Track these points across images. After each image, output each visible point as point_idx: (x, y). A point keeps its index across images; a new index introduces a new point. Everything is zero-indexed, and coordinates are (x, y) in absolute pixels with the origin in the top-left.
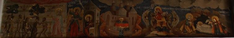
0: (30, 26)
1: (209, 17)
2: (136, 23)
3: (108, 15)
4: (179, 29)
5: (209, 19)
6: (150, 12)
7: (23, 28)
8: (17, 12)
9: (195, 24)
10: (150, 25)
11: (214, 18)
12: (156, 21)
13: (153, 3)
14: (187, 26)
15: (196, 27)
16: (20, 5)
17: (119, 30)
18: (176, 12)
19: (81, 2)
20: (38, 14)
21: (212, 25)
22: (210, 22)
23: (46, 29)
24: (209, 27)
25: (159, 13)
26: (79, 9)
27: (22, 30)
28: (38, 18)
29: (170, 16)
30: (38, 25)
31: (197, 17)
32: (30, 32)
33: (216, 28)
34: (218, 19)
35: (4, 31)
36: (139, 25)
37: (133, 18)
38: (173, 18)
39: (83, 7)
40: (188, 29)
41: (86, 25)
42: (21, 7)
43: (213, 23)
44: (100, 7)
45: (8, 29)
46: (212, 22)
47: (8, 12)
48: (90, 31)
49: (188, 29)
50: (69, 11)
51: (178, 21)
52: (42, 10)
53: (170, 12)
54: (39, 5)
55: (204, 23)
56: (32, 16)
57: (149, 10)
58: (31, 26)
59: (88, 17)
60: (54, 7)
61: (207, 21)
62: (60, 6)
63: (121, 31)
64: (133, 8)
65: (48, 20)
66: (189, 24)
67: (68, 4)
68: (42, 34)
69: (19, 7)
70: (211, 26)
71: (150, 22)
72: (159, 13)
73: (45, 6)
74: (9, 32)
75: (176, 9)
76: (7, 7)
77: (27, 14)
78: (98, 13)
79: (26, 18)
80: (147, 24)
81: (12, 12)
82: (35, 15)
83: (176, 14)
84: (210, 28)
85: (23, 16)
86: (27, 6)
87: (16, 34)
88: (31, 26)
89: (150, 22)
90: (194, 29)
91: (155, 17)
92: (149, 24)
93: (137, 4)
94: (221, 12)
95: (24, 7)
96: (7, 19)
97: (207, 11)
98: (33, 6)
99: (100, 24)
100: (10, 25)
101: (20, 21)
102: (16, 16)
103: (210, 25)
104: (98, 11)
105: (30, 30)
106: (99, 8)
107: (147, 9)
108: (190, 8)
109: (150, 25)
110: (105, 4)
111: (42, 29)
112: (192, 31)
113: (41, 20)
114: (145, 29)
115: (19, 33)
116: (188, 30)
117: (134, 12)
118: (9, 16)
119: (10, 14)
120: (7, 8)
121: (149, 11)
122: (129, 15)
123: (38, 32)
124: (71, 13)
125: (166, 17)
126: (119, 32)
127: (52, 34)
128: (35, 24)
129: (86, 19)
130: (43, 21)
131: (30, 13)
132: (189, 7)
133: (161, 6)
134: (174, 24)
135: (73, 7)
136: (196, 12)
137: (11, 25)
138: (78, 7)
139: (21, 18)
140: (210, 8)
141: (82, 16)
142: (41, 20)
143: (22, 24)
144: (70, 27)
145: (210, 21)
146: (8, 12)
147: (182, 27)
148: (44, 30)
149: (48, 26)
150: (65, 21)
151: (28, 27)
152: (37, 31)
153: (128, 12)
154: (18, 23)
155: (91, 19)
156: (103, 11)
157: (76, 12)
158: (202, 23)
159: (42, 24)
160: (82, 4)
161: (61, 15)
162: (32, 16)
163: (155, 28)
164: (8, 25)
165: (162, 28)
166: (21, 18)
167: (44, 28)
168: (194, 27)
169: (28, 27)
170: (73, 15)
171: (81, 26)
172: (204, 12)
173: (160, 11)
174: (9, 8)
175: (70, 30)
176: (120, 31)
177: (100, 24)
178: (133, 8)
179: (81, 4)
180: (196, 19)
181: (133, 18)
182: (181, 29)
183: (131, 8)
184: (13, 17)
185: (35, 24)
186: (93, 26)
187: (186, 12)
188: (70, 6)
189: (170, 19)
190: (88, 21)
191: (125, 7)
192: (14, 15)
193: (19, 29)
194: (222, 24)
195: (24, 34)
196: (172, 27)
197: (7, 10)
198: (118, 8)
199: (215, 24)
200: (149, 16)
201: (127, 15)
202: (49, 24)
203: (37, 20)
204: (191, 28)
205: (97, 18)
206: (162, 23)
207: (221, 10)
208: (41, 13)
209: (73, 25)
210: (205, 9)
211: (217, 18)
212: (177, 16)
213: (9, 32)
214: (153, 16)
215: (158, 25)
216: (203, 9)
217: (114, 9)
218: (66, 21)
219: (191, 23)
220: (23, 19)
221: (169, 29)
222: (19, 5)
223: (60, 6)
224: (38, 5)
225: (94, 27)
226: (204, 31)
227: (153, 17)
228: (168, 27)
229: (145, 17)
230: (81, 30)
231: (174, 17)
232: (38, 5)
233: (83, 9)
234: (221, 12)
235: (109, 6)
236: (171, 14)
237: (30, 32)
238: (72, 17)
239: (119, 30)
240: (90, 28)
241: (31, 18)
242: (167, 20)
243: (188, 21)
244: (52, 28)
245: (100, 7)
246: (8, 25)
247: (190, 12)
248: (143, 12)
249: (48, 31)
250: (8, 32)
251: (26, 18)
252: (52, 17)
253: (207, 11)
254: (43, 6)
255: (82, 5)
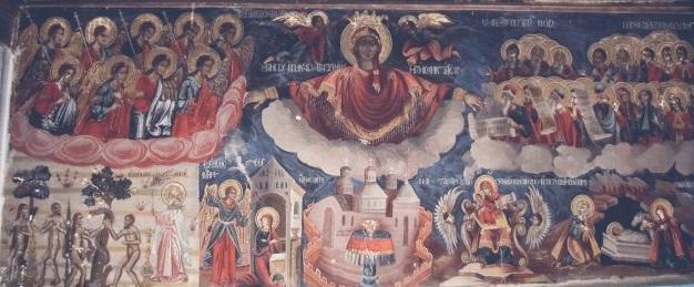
0: (86, 242)
1: (643, 205)
2: (416, 236)
3: (329, 210)
4: (550, 253)
5: (643, 211)
6: (459, 197)
7: (68, 249)
8: (46, 193)
9: (599, 229)
10: (460, 241)
11: (658, 209)
12: (477, 228)
13: (472, 161)
14: (575, 243)
15: (600, 244)
16: (54, 168)
17: (362, 262)
18: (541, 192)
19: (243, 162)
20: (109, 201)
21: (652, 233)
22: (645, 222)
23: (136, 254)
24: (642, 238)
25: (487, 198)
26: (172, 59)
27: (65, 257)
28: (109, 216)
29: (521, 210)
30: (110, 240)
31: (605, 207)
32: (90, 265)
33: (663, 243)
34: (670, 211)
35: (9, 259)
36: (425, 244)
37: (406, 220)
38: (532, 215)
39: (248, 179)
40: (576, 250)
41: (260, 245)
42: (58, 176)
43: (657, 225)
44: (303, 180)
45: (20, 252)
46: (650, 220)
47: (18, 194)
48: (272, 266)
49: (576, 250)
50: (206, 194)
51: (547, 224)
52: (121, 189)
53: (522, 193)
54: (112, 170)
55: (627, 226)
56: (92, 208)
57: (459, 190)
58: (90, 243)
59: (265, 217)
60: (157, 180)
61: (637, 219)
62: (176, 174)
63: (368, 266)
64: (407, 183)
65: (142, 222)
66: (582, 233)
67: (202, 170)
68: (124, 273)
69: (50, 175)
70: (649, 237)
71: (459, 231)
72: (489, 200)
73: (129, 175)
74: (24, 262)
75: (542, 182)
76: (18, 174)
77: (78, 203)
78: (296, 203)
79: (72, 216)
80: (450, 239)
81: (32, 195)
82: (101, 203)
83: (541, 198)
84: (646, 243)
85: (64, 208)
86: (77, 173)
87: (44, 269)
88: (90, 243)
89: (459, 231)
90: (596, 251)
91: (477, 213)
92: (455, 241)
93: (420, 170)
94: (680, 185)
95: (67, 176)
96: (18, 217)
97: (639, 183)
98: (94, 175)
99: (305, 241)
100: (26, 239)
101: (58, 226)
102: (44, 205)
103: (646, 232)
104: (295, 196)
105: (89, 254)
106: (301, 185)
107: (452, 187)
108: (586, 177)
109: (460, 241)
110: (318, 171)
111: (125, 253)
112: (588, 256)
113: (118, 226)
114: (443, 259)
115: (56, 265)
116: (577, 255)
117: (409, 201)
118: (22, 206)
119: (26, 201)
120: (16, 181)
121: (459, 193)
122: (394, 210)
123: (111, 263)
124: (211, 202)
125: (509, 213)
126: (362, 269)
127: (155, 271)
128: (103, 236)
129: (259, 225)
130: (127, 227)
131: (86, 197)
132: (584, 172)
133: (499, 174)
134: (535, 236)
135: (217, 180)
136: (604, 188)
137: (30, 239)
138: (147, 15)
139: (59, 214)
140: (647, 171)
141: (247, 212)
142: (118, 226)
143: (62, 236)
144: (212, 251)
145: (646, 218)
146: (18, 194)
147: (558, 247)
148: (129, 256)
149: (143, 245)
150: (193, 229)
151: (82, 245)
152: (108, 261)
153: (392, 196)
154: (50, 230)
155: (275, 224)
156: (312, 194)
157: (225, 199)
158: (621, 228)
159: (123, 237)
160: (247, 169)
161: (181, 207)
162: (92, 208)
163: (475, 254)
164: (20, 237)
165: (495, 252)
166: (59, 214)
167: (130, 251)
168: (594, 244)
169: (82, 245)
170: (217, 210)
171: (245, 246)
172: (629, 189)
173: (492, 191)
174: (22, 180)
175: (209, 261)
176: (366, 266)
177: (305, 241)
178: (407, 183)
179: (242, 168)
180: (602, 216)
181: (406, 220)
182: (556, 253)
183: (400, 184)
184: (34, 211)
185: (103, 236)
186: (281, 248)
187: (572, 191)
188: (208, 175)
189: (523, 220)
190: (266, 229)
191: (383, 182)
192: (37, 203)
193: (53, 252)
194: (682, 226)
195: (70, 271)
196: (526, 247)
197: (15, 186)
198: (360, 186)
199: (662, 227)
200: (456, 211)
201: (389, 212)
202: (144, 238)
203: (107, 222)
204: (586, 246)
205: (292, 220)
206: (495, 235)
207: (682, 178)
208: (119, 198)
209: (218, 250)
210: (632, 176)
211: (667, 205)
212: (545, 206)
213: (24, 262)
214: (470, 210)
215: (485, 242)
216: (624, 178)
217: (348, 187)
218: (197, 226)
219: (586, 229)
220: (65, 216)
221: (519, 256)
222: (52, 170)
223: (176, 174)
224: (107, 170)
225: (284, 250)
226: (627, 256)
227: (470, 213)
228: (516, 250)
229: (446, 216)
230: (244, 264)
231: (534, 212)
232: (107, 170)
233: (249, 187)
234: (680, 185)
235: (332, 179)
236: (527, 199)
237: (86, 264)
238: (217, 216)
239: (362, 262)
240: (275, 257)
241: (90, 216)
242: (512, 225)
243: (579, 222)
244: (154, 251)
245: (303, 180)
246: (20, 237)
247: (585, 190)
248: (438, 196)
249: (140, 264)
250: (21, 261)
251: (72, 216)
252: (153, 212)
253: (639, 183)
254: (125, 172)
255: (244, 172)
